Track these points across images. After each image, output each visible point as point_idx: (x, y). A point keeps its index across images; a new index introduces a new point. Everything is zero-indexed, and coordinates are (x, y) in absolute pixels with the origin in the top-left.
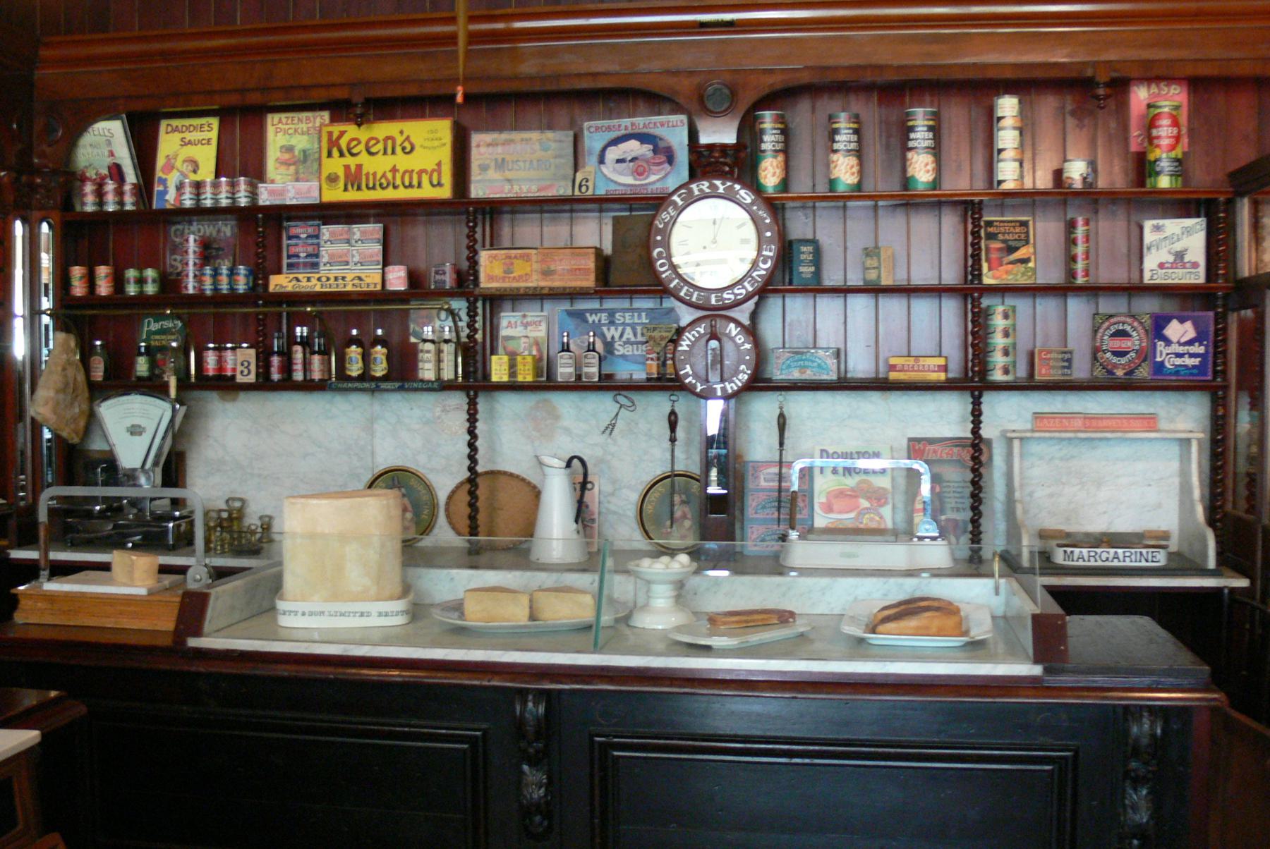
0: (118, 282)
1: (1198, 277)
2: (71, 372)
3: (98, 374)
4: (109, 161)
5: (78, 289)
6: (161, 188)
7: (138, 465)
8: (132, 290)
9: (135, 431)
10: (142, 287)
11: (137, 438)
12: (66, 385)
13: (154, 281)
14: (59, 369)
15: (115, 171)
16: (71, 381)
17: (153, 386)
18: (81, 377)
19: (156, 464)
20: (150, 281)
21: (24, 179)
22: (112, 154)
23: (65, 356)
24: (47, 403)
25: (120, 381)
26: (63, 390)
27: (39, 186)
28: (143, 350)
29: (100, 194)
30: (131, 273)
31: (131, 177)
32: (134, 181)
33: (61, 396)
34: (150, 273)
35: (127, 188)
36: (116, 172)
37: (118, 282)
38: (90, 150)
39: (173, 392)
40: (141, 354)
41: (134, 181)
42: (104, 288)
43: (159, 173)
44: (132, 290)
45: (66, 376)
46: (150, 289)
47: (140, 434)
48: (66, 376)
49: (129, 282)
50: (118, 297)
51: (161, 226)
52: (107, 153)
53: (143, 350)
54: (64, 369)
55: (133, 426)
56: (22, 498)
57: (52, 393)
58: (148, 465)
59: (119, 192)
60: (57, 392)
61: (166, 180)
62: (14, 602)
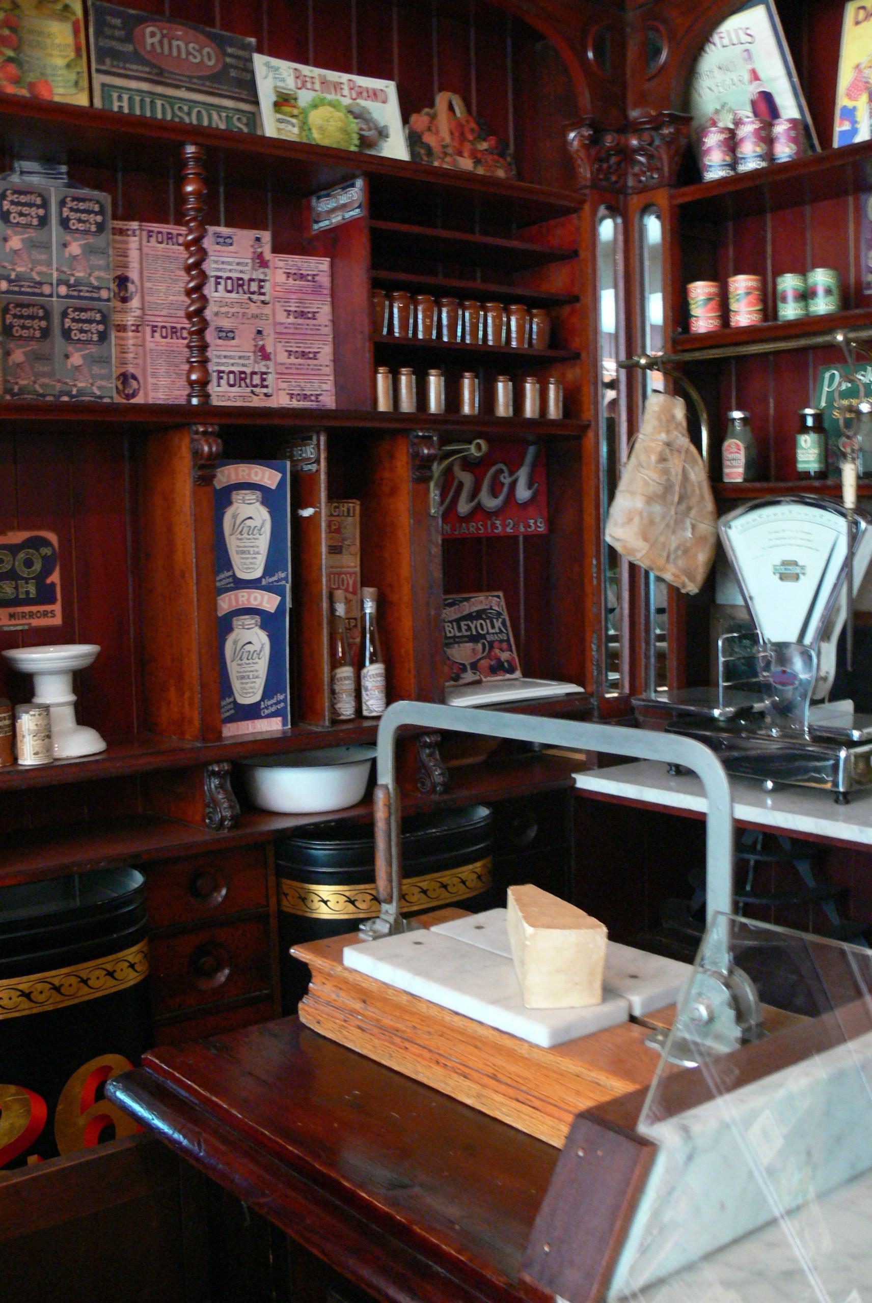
0: (769, 301)
1: (280, 719)
2: (676, 465)
3: (736, 469)
4: (752, 90)
5: (703, 321)
6: (846, 126)
7: (792, 637)
8: (790, 311)
9: (789, 572)
10: (807, 307)
11: (789, 585)
12: (668, 488)
13: (828, 292)
14: (654, 458)
15: (763, 107)
16: (677, 480)
17: (821, 490)
18: (698, 474)
19: (824, 634)
20: (820, 292)
21: (609, 140)
22: (755, 76)
23: (663, 436)
24: (630, 520)
25: (773, 479)
26: (662, 495)
27: (636, 151)
28: (810, 422)
29: (732, 143)
30: (789, 283)
31: (789, 107)
32: (795, 114)
33: (657, 509)
34: (821, 277)
35: (780, 128)
36: (766, 106)
37: (769, 301)
38: (719, 76)
39: (849, 497)
40: (805, 429)
41: (795, 114)
42: (744, 314)
43: (842, 101)
44: (790, 311)
45: (666, 472)
46: (822, 306)
47: (797, 578)
48: (666, 472)
49: (784, 300)
50: (770, 323)
51: (851, 199)
52: (746, 77)
53: (810, 422)
54: (663, 459)
55: (784, 563)
56: (615, 685)
57: (639, 503)
58: (808, 639)
59: (767, 139)
60: (650, 500)
61: (855, 108)
62: (299, 979)
